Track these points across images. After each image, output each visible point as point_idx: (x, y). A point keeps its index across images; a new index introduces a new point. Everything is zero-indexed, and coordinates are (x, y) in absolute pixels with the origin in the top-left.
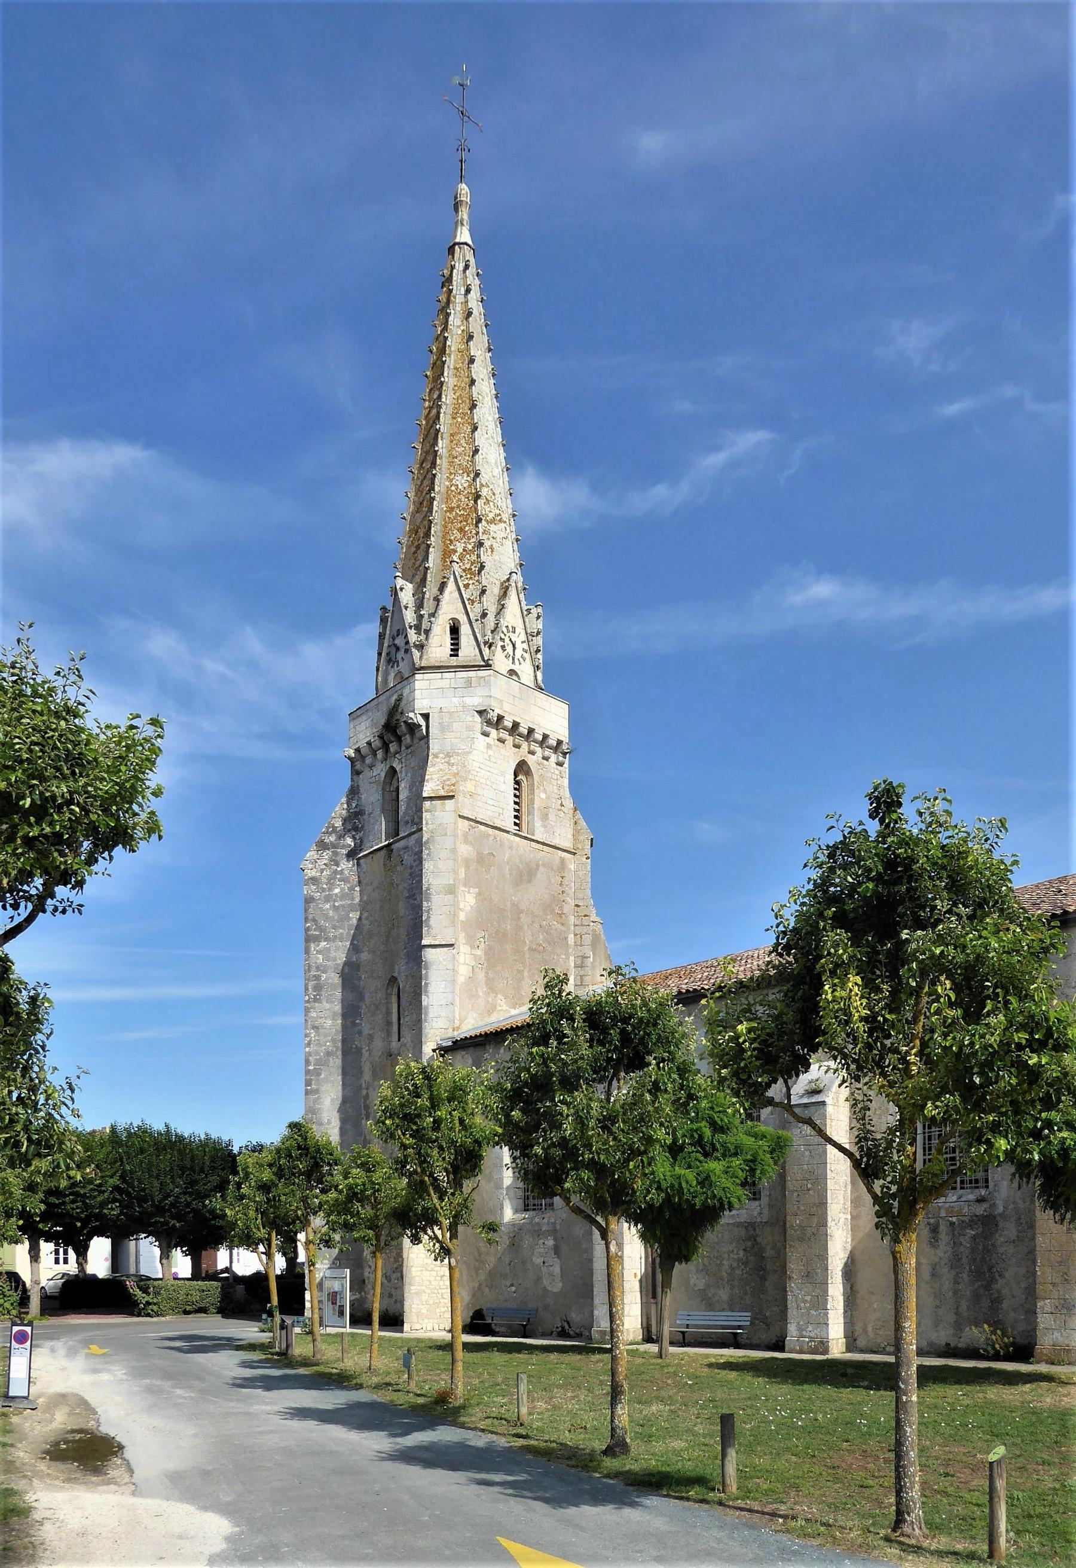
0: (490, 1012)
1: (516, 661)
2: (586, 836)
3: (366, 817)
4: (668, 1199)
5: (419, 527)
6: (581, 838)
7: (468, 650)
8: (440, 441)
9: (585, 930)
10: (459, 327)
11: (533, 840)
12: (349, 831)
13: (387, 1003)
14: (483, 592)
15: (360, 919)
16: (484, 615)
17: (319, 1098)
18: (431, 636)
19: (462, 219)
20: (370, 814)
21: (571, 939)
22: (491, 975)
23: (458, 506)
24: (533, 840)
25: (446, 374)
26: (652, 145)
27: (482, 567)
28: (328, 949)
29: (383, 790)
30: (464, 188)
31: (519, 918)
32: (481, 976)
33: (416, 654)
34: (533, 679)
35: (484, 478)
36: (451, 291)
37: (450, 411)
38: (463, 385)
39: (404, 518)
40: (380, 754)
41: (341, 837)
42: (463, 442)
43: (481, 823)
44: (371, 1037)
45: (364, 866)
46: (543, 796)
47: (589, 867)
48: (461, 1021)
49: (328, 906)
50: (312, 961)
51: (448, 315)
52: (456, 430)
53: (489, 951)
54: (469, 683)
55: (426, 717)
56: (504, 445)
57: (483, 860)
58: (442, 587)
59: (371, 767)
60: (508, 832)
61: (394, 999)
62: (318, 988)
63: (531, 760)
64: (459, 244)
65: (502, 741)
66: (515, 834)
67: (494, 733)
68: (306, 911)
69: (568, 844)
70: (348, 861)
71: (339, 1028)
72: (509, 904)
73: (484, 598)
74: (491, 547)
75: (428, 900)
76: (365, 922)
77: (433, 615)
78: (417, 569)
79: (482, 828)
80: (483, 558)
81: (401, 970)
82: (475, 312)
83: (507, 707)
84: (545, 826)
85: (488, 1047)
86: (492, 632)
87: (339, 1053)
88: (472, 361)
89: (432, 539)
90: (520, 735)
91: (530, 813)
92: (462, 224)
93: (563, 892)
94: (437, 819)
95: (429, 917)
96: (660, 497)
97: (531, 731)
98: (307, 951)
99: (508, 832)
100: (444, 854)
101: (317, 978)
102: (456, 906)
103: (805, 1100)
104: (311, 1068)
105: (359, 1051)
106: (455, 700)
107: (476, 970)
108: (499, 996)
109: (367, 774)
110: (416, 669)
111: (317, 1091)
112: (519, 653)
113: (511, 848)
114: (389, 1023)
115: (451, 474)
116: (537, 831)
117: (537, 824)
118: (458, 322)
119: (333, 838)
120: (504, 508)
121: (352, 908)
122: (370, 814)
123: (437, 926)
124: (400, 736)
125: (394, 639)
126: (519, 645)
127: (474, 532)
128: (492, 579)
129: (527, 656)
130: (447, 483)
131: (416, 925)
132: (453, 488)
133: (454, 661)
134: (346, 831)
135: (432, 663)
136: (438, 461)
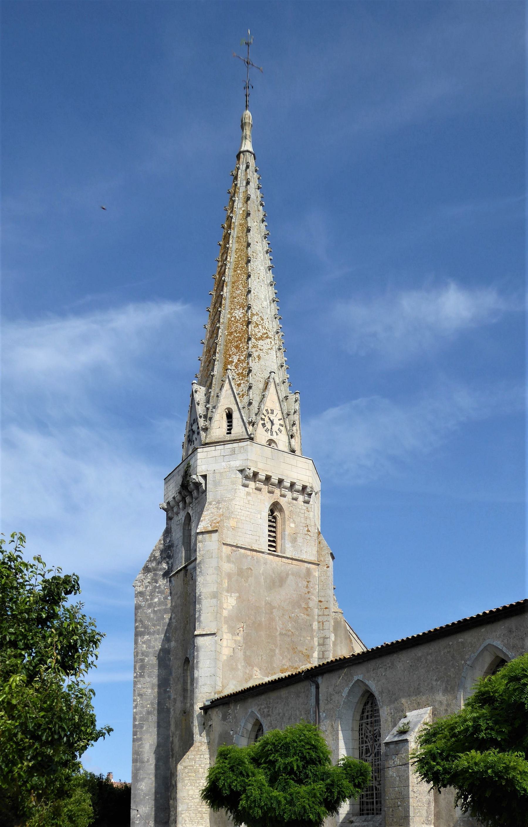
0: (247, 681)
1: (274, 434)
2: (327, 551)
3: (175, 548)
4: (265, 813)
5: (211, 348)
6: (323, 553)
7: (238, 428)
8: (225, 288)
9: (325, 618)
10: (241, 208)
11: (284, 557)
12: (165, 558)
13: (184, 676)
14: (250, 388)
15: (171, 619)
16: (250, 404)
18: (213, 421)
19: (246, 135)
21: (315, 625)
22: (248, 653)
23: (236, 331)
24: (284, 557)
25: (231, 242)
27: (250, 371)
28: (150, 640)
29: (184, 529)
30: (248, 113)
32: (240, 654)
33: (203, 434)
34: (287, 444)
35: (255, 308)
36: (236, 185)
37: (232, 267)
39: (203, 343)
41: (159, 563)
42: (241, 287)
43: (241, 548)
45: (173, 582)
46: (293, 525)
49: (150, 611)
50: (139, 648)
51: (234, 202)
52: (236, 278)
53: (247, 639)
59: (177, 514)
60: (263, 553)
62: (143, 667)
63: (283, 502)
64: (243, 152)
65: (259, 489)
66: (269, 554)
67: (252, 484)
68: (136, 614)
70: (163, 579)
71: (156, 694)
72: (263, 603)
73: (251, 392)
74: (259, 357)
75: (200, 603)
76: (174, 621)
78: (208, 377)
80: (251, 364)
82: (253, 197)
84: (293, 547)
85: (231, 705)
86: (256, 415)
87: (156, 712)
88: (248, 230)
89: (217, 355)
90: (273, 484)
91: (283, 538)
92: (246, 138)
93: (308, 592)
95: (200, 615)
97: (281, 481)
99: (263, 553)
100: (211, 571)
101: (142, 660)
103: (396, 739)
104: (137, 723)
105: (168, 710)
106: (223, 464)
107: (236, 650)
108: (255, 668)
109: (176, 519)
111: (140, 739)
112: (275, 428)
113: (265, 563)
115: (232, 309)
117: (287, 546)
118: (240, 205)
119: (154, 564)
121: (165, 611)
124: (189, 493)
125: (192, 426)
126: (277, 422)
127: (246, 347)
129: (283, 429)
130: (229, 316)
132: (233, 319)
133: (228, 437)
136: (223, 302)
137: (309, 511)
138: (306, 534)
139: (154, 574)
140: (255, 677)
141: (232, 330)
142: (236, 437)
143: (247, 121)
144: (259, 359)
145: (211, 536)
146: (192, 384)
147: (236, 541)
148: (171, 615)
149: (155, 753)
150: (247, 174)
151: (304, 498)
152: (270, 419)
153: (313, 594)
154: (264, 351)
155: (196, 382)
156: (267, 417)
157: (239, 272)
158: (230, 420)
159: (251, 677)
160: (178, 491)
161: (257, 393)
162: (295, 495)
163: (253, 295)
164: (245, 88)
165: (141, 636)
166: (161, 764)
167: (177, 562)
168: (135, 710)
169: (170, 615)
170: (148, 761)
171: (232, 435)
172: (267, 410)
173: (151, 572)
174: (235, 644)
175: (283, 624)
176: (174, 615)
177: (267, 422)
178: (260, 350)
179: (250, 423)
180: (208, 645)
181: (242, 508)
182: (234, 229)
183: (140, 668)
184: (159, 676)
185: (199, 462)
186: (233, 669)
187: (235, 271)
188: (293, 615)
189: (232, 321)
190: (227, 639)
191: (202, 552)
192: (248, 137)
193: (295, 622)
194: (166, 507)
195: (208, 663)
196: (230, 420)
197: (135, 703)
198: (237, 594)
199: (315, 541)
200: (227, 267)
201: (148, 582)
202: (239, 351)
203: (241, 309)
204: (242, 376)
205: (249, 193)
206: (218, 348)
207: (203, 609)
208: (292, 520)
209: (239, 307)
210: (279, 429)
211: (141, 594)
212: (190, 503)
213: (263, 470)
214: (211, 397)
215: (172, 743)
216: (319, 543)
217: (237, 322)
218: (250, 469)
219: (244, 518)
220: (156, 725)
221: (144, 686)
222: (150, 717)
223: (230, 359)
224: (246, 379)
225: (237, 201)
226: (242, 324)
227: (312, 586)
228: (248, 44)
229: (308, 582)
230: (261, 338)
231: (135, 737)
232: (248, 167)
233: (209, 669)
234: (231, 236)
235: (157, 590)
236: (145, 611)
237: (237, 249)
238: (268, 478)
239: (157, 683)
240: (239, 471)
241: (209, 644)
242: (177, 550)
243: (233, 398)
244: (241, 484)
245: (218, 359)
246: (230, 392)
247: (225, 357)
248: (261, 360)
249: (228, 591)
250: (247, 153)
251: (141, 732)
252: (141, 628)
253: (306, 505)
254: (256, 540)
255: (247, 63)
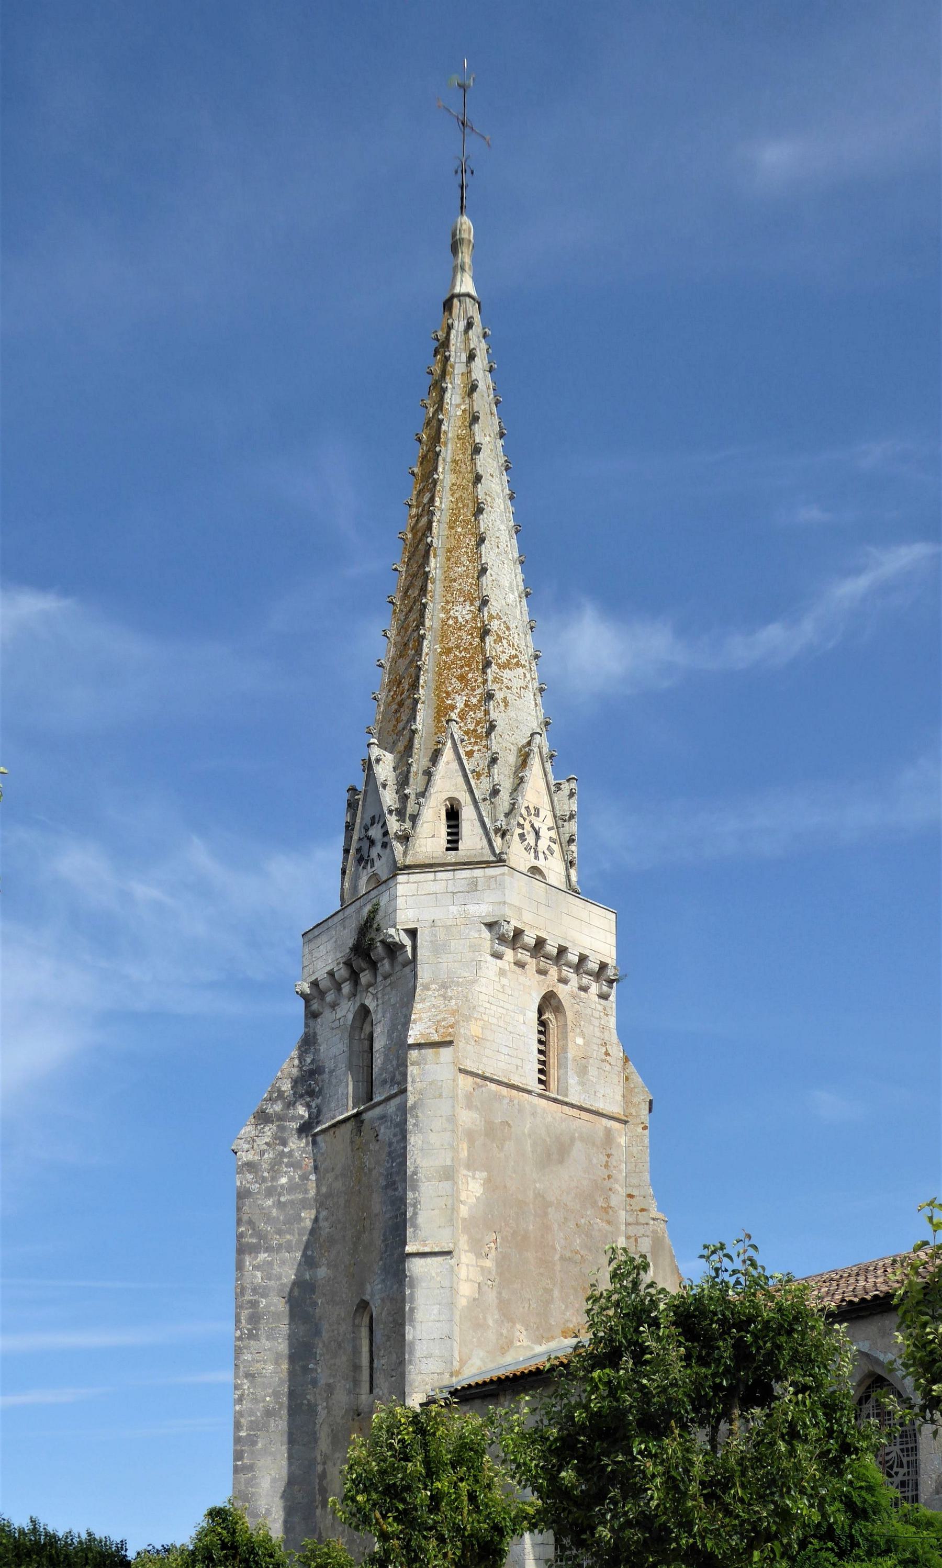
0: (504, 1350)
1: (541, 855)
2: (642, 1096)
3: (326, 1076)
6: (635, 1100)
7: (472, 840)
9: (641, 1230)
10: (458, 406)
11: (566, 1104)
12: (301, 1096)
13: (354, 1339)
14: (494, 760)
15: (316, 1220)
16: (495, 792)
17: (254, 1477)
18: (420, 822)
20: (331, 1072)
22: (505, 1295)
23: (458, 647)
24: (566, 1104)
25: (440, 469)
26: (776, 160)
27: (492, 727)
28: (270, 1264)
29: (351, 1038)
31: (546, 1214)
32: (491, 1296)
33: (398, 848)
35: (495, 606)
37: (446, 518)
38: (465, 482)
39: (381, 666)
40: (346, 988)
41: (290, 1105)
42: (464, 559)
43: (492, 1080)
44: (330, 1388)
45: (322, 1145)
46: (580, 1041)
47: (647, 1141)
48: (463, 1362)
51: (443, 391)
52: (454, 542)
53: (503, 1262)
54: (473, 886)
55: (412, 933)
56: (522, 563)
57: (495, 1132)
58: (436, 756)
59: (333, 1006)
60: (529, 1092)
61: (364, 1332)
62: (255, 1319)
63: (563, 992)
64: (459, 296)
65: (520, 965)
67: (509, 954)
68: (239, 1209)
69: (615, 1109)
70: (299, 1138)
71: (285, 1375)
72: (531, 1194)
73: (495, 770)
74: (505, 700)
75: (415, 1189)
76: (323, 1224)
77: (422, 794)
78: (400, 733)
79: (493, 1086)
80: (493, 715)
81: (375, 1291)
82: (481, 385)
83: (528, 917)
84: (582, 1084)
87: (284, 1412)
89: (421, 691)
91: (562, 1065)
92: (463, 269)
93: (609, 1177)
94: (427, 1074)
96: (775, 641)
97: (562, 950)
98: (240, 1266)
99: (529, 1092)
101: (254, 1304)
102: (454, 1196)
104: (243, 1434)
105: (312, 1410)
106: (453, 909)
107: (485, 1288)
108: (518, 1326)
109: (328, 1016)
110: (397, 869)
111: (250, 1468)
112: (543, 844)
113: (534, 1114)
114: (356, 1368)
115: (447, 602)
116: (572, 1091)
118: (457, 399)
119: (278, 1107)
120: (523, 647)
121: (304, 1204)
122: (331, 1072)
123: (427, 1227)
124: (374, 958)
125: (367, 830)
126: (544, 833)
127: (480, 680)
128: (506, 743)
129: (556, 847)
131: (398, 1226)
132: (451, 622)
133: (452, 857)
134: (298, 1096)
135: (421, 859)
137: (607, 1015)
138: (603, 1061)
139: (278, 1126)
140: (519, 1344)
141: (450, 644)
142: (468, 858)
143: (465, 236)
144: (506, 705)
145: (438, 1053)
146: (369, 745)
147: (482, 1066)
148: (318, 1212)
149: (284, 1496)
150: (469, 339)
151: (601, 988)
152: (532, 826)
153: (616, 1181)
154: (515, 691)
155: (376, 741)
156: (527, 821)
157: (459, 530)
158: (452, 823)
159: (507, 1345)
160: (344, 960)
161: (506, 773)
162: (586, 980)
163: (490, 578)
164: (456, 172)
165: (250, 1254)
166: (296, 1519)
167: (333, 1105)
168: (238, 1408)
169: (314, 1212)
170: (268, 1511)
171: (459, 852)
172: (527, 808)
173: (272, 1122)
174: (483, 1275)
175: (566, 1239)
176: (324, 1213)
177: (529, 833)
178: (507, 687)
179: (497, 831)
180: (434, 1274)
181: (492, 1000)
182: (446, 444)
183: (251, 1320)
184: (291, 1337)
185: (400, 902)
186: (479, 1326)
187: (451, 528)
188: (583, 1221)
189: (449, 626)
190: (467, 1265)
191: (418, 1085)
192: (467, 268)
193: (586, 1236)
194: (308, 991)
195: (435, 1311)
196: (452, 823)
197: (239, 1392)
198: (485, 1174)
199: (619, 1076)
200: (435, 519)
201: (266, 1143)
202: (466, 685)
203: (468, 603)
204: (476, 737)
205: (474, 377)
206: (422, 677)
207: (422, 1200)
208: (578, 1030)
209: (462, 599)
210: (549, 848)
211: (250, 1166)
212: (370, 985)
213: (532, 927)
214: (412, 775)
215: (323, 1476)
216: (627, 1079)
217: (460, 629)
218: (508, 922)
219: (494, 1021)
220: (285, 1439)
221: (257, 1357)
222: (272, 1421)
223: (449, 702)
224: (484, 743)
225: (449, 391)
226: (472, 634)
227: (615, 1164)
228: (463, 87)
229: (608, 1156)
230: (505, 666)
231: (239, 1463)
232: (469, 325)
233: (438, 1325)
234: (440, 458)
235: (286, 1160)
236: (259, 1202)
237: (453, 485)
238: (540, 943)
239: (286, 1352)
240: (485, 924)
241: (437, 1274)
242: (334, 1081)
243: (461, 780)
244: (488, 951)
245: (423, 698)
246: (455, 765)
247: (438, 696)
248: (509, 708)
249: (468, 1167)
250: (468, 299)
251: (252, 1453)
252: (251, 1236)
253: (602, 1001)
254: (517, 1066)
255: (463, 124)
